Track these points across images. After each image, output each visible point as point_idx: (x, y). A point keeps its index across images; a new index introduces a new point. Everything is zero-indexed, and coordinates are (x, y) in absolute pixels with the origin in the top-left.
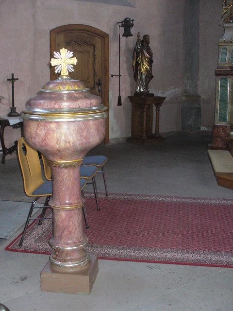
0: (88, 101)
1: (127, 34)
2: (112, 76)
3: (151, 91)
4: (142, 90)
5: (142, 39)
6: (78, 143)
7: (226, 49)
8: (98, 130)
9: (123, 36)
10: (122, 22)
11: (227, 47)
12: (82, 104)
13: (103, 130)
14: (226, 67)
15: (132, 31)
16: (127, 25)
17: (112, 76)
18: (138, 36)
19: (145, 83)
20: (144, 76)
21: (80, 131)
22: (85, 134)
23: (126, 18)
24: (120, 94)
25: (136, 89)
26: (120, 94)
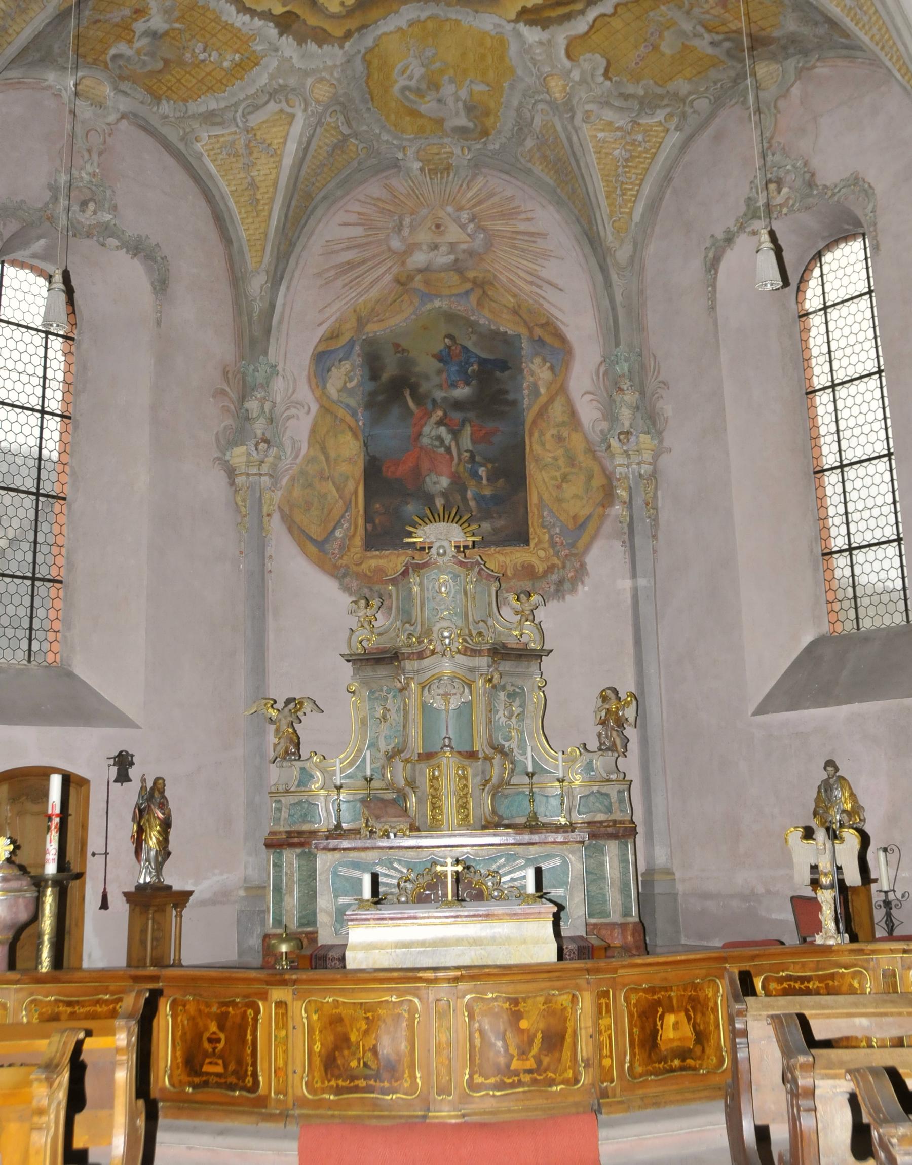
0: (20, 882)
1: (123, 777)
2: (94, 855)
3: (167, 882)
4: (148, 879)
5: (149, 785)
6: (8, 918)
7: (280, 801)
8: (26, 906)
9: (115, 781)
10: (115, 758)
11: (280, 798)
12: (14, 884)
13: (32, 907)
14: (280, 832)
15: (132, 772)
16: (123, 762)
17: (94, 855)
18: (143, 780)
19: (156, 865)
20: (153, 853)
21: (10, 907)
22: (14, 910)
23: (121, 752)
24: (105, 889)
25: (139, 878)
26: (105, 889)
